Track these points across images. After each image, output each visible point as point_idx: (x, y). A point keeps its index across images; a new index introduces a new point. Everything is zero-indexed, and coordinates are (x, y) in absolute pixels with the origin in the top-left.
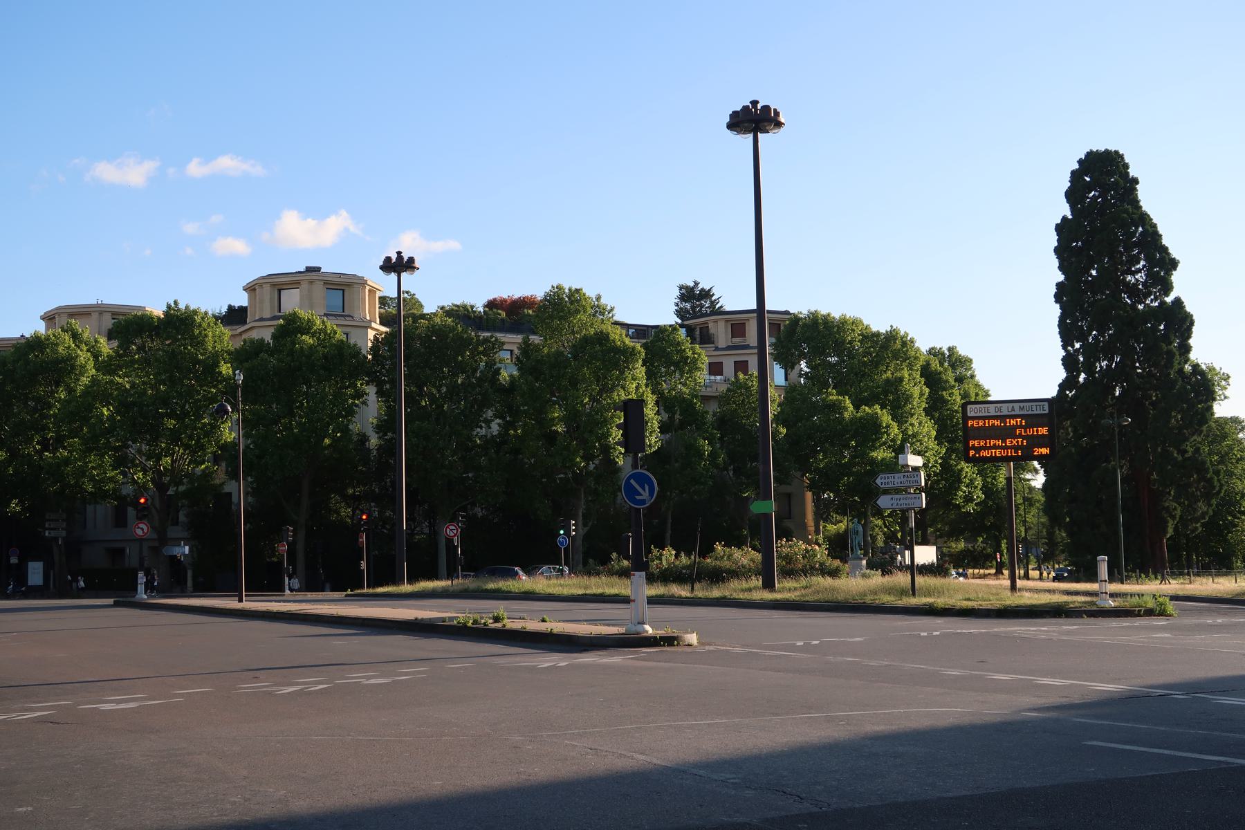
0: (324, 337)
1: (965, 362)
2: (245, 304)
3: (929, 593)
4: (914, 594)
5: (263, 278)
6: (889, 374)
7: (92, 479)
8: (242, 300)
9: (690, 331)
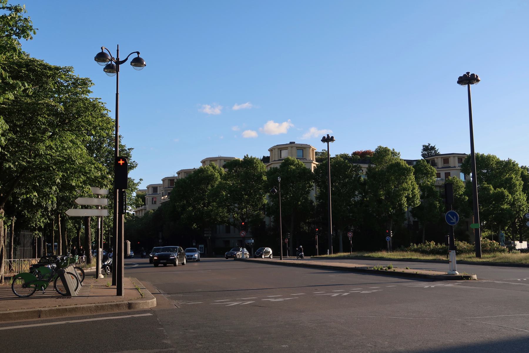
0: (298, 166)
2: (269, 155)
6: (507, 176)
7: (220, 216)
8: (268, 154)
9: (428, 162)
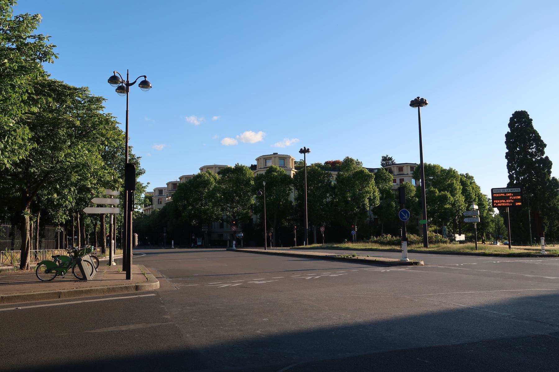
1: (471, 178)
3: (481, 249)
8: (255, 163)
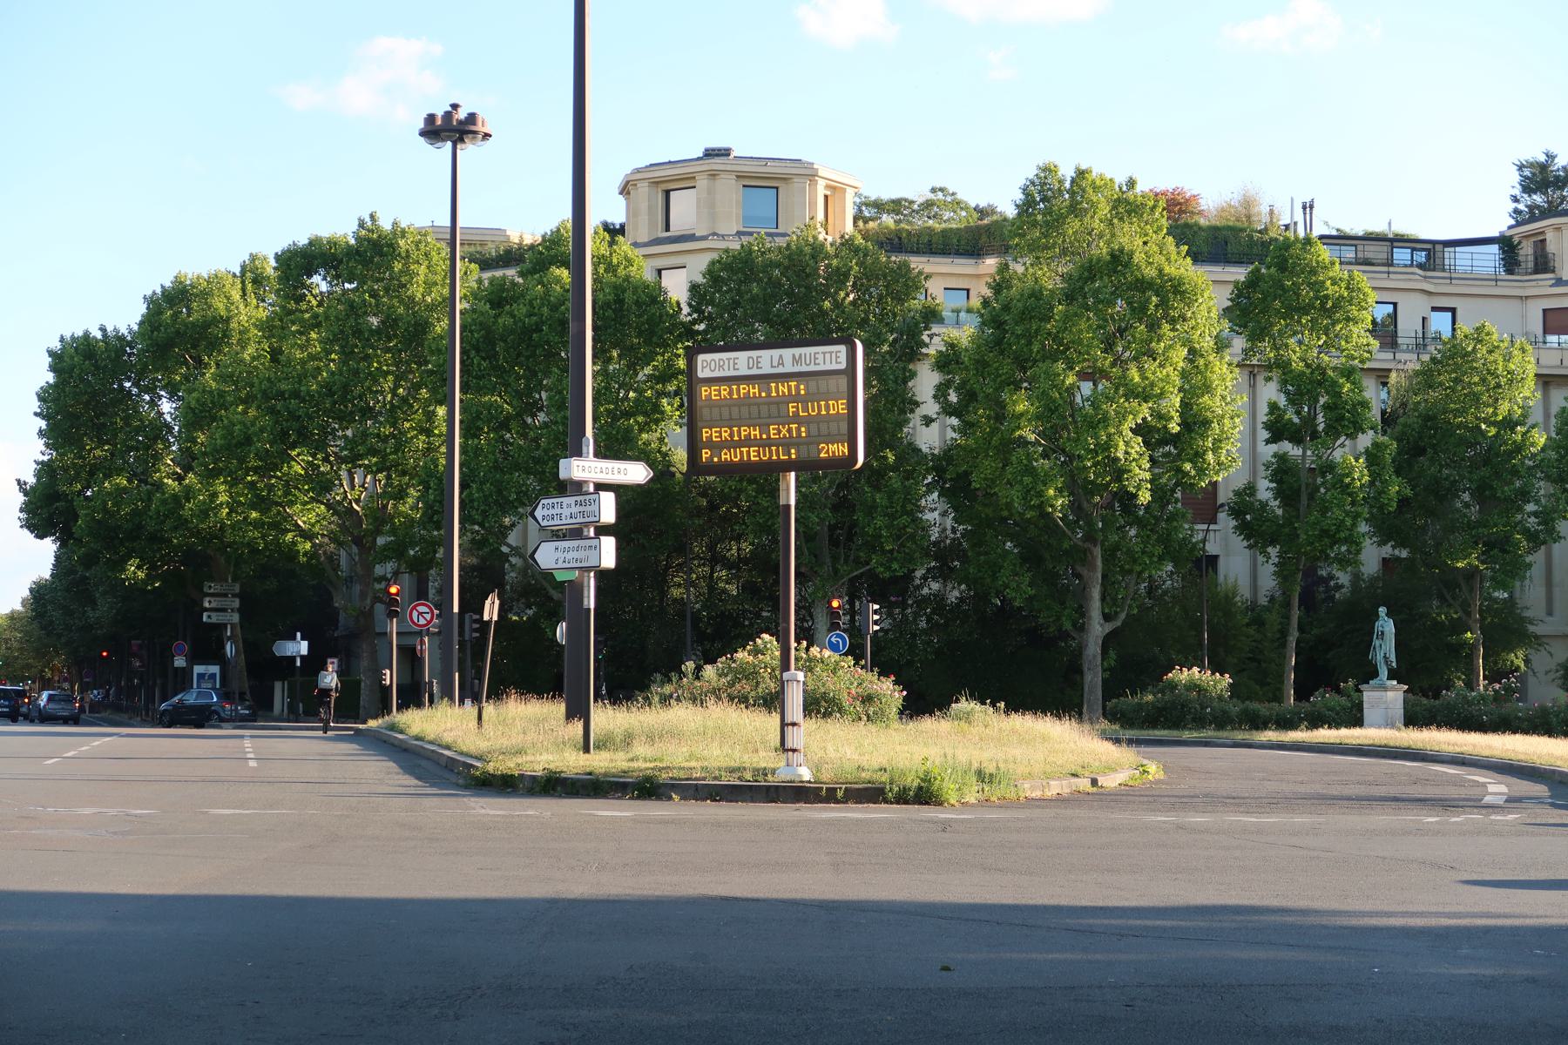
4: (586, 749)
5: (638, 171)
